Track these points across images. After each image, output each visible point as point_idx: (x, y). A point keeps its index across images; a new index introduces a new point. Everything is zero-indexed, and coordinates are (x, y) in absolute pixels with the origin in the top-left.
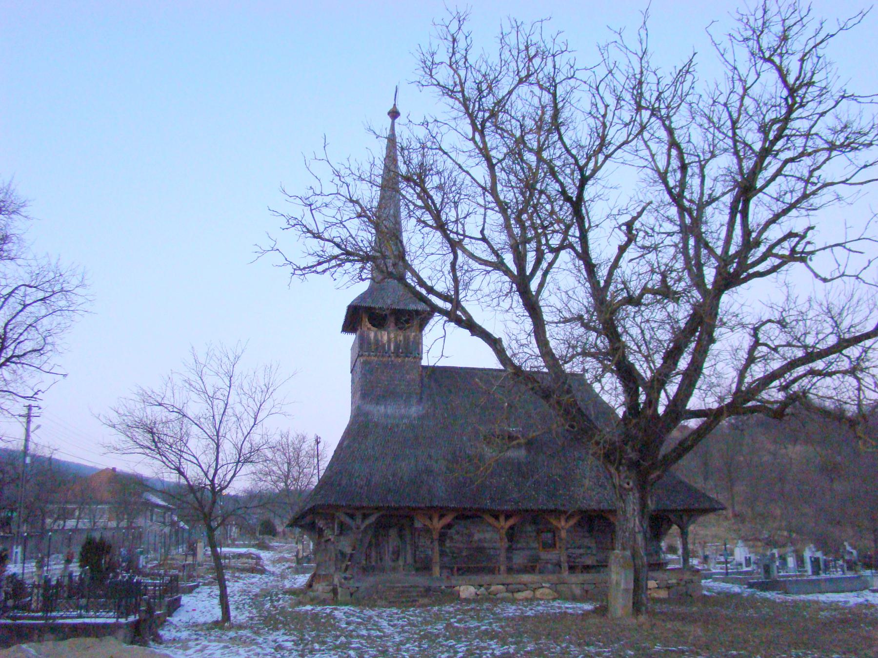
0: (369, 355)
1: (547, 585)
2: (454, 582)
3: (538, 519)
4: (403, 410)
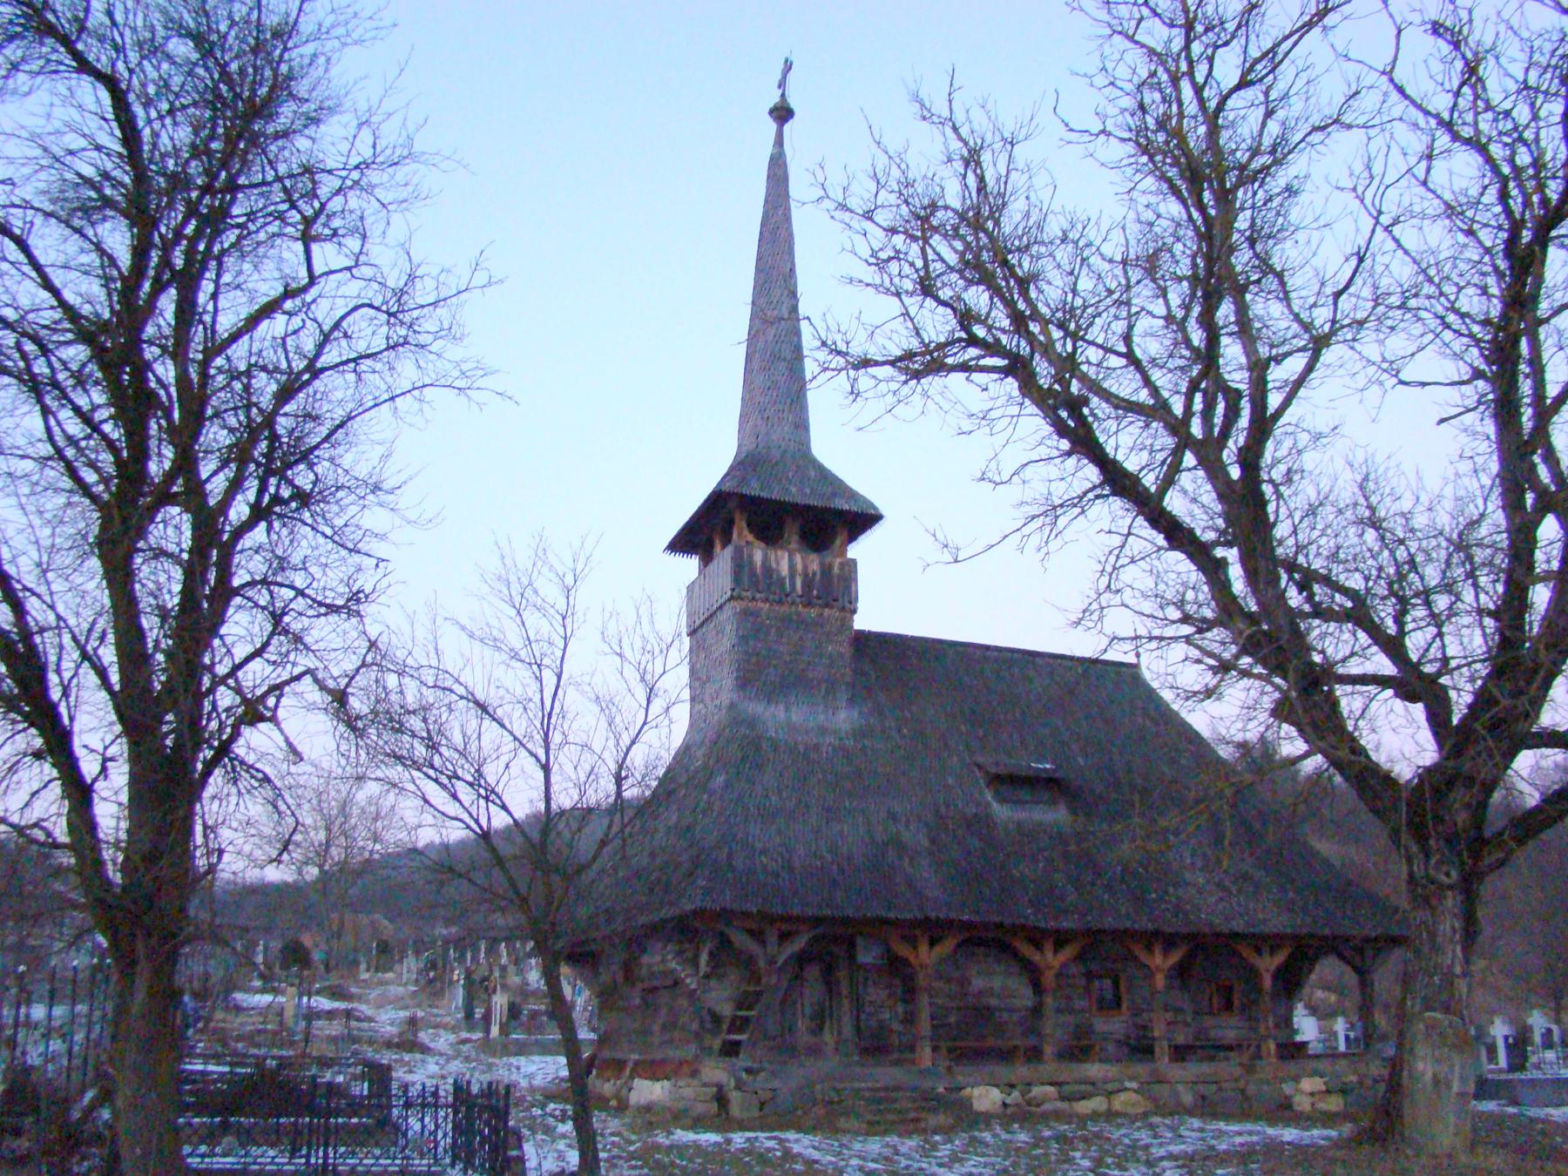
0: (753, 599)
1: (1134, 1085)
3: (1104, 952)
4: (822, 717)
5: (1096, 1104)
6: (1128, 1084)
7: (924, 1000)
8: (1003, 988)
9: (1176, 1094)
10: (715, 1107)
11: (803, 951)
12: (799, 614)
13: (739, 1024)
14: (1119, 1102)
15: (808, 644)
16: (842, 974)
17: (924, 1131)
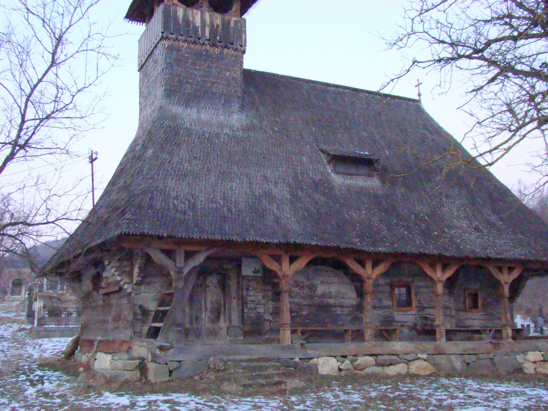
1: (424, 356)
2: (310, 352)
3: (405, 267)
5: (400, 368)
6: (419, 355)
8: (338, 292)
9: (450, 362)
11: (202, 266)
12: (207, 51)
13: (160, 316)
14: (414, 367)
15: (213, 71)
16: (233, 284)
17: (282, 393)
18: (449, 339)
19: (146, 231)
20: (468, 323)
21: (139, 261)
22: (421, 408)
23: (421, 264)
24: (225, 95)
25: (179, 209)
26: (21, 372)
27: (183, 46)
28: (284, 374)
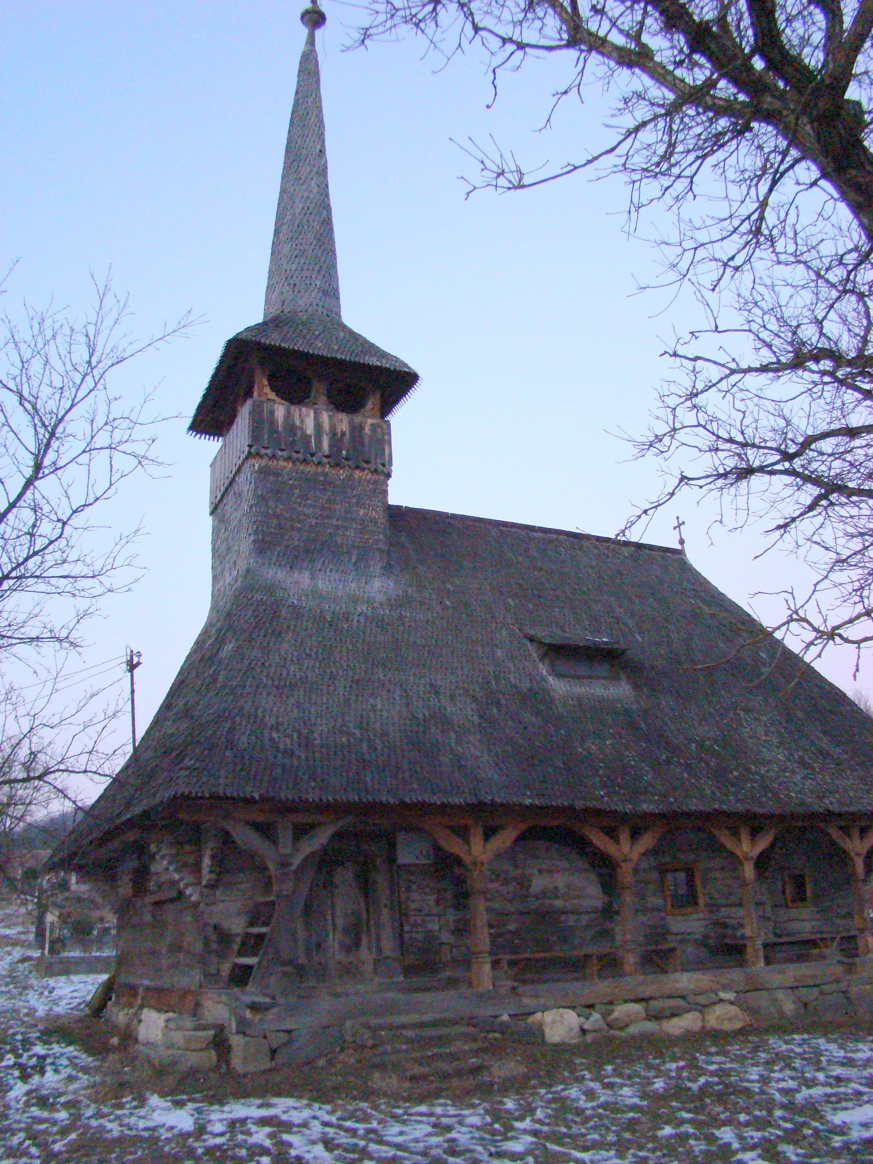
0: (274, 456)
3: (687, 836)
5: (688, 1022)
6: (722, 995)
7: (480, 909)
10: (213, 1054)
11: (324, 851)
12: (326, 475)
13: (253, 944)
16: (381, 880)
17: (485, 1090)
18: (768, 961)
19: (221, 791)
20: (791, 926)
21: (211, 845)
22: (758, 1113)
23: (717, 833)
24: (358, 548)
25: (282, 747)
26: (8, 1047)
27: (285, 468)
28: (484, 1050)
